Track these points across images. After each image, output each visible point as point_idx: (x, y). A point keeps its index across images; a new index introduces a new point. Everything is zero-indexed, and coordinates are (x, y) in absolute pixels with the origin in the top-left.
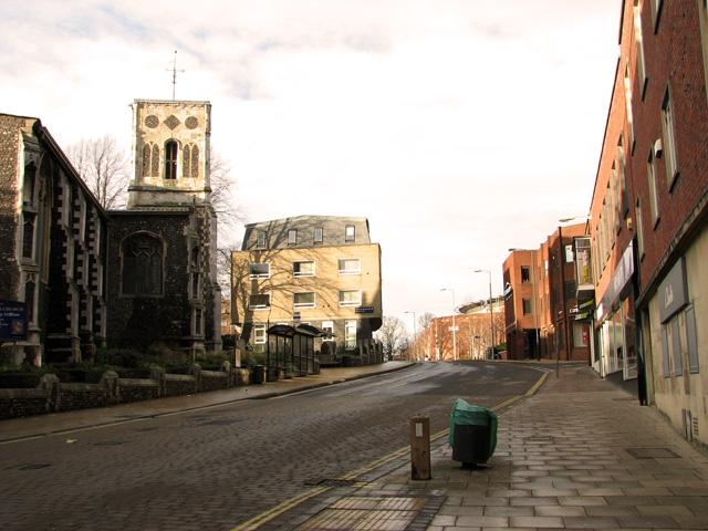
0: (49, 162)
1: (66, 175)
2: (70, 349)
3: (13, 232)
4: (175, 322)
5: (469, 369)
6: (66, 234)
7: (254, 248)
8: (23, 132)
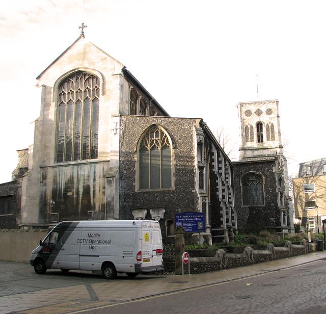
0: (208, 142)
1: (215, 145)
2: (223, 236)
3: (194, 177)
4: (272, 219)
5: (75, 203)
6: (217, 176)
7: (305, 176)
8: (195, 126)
